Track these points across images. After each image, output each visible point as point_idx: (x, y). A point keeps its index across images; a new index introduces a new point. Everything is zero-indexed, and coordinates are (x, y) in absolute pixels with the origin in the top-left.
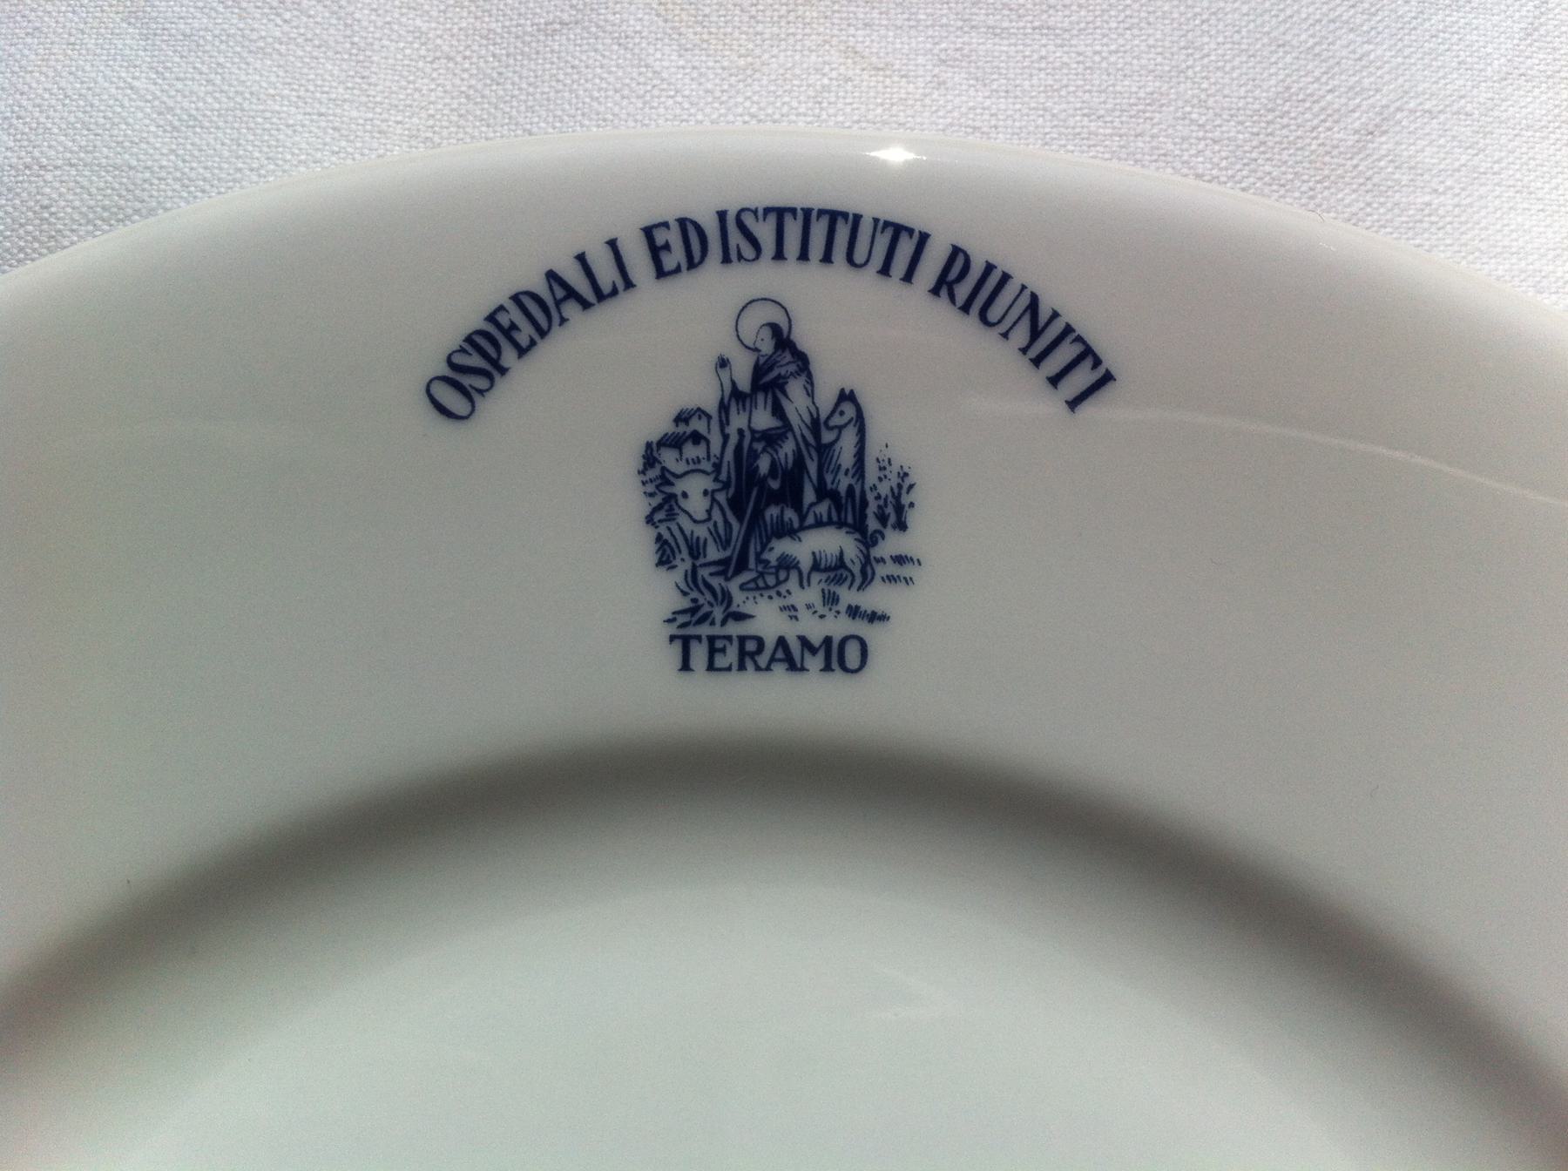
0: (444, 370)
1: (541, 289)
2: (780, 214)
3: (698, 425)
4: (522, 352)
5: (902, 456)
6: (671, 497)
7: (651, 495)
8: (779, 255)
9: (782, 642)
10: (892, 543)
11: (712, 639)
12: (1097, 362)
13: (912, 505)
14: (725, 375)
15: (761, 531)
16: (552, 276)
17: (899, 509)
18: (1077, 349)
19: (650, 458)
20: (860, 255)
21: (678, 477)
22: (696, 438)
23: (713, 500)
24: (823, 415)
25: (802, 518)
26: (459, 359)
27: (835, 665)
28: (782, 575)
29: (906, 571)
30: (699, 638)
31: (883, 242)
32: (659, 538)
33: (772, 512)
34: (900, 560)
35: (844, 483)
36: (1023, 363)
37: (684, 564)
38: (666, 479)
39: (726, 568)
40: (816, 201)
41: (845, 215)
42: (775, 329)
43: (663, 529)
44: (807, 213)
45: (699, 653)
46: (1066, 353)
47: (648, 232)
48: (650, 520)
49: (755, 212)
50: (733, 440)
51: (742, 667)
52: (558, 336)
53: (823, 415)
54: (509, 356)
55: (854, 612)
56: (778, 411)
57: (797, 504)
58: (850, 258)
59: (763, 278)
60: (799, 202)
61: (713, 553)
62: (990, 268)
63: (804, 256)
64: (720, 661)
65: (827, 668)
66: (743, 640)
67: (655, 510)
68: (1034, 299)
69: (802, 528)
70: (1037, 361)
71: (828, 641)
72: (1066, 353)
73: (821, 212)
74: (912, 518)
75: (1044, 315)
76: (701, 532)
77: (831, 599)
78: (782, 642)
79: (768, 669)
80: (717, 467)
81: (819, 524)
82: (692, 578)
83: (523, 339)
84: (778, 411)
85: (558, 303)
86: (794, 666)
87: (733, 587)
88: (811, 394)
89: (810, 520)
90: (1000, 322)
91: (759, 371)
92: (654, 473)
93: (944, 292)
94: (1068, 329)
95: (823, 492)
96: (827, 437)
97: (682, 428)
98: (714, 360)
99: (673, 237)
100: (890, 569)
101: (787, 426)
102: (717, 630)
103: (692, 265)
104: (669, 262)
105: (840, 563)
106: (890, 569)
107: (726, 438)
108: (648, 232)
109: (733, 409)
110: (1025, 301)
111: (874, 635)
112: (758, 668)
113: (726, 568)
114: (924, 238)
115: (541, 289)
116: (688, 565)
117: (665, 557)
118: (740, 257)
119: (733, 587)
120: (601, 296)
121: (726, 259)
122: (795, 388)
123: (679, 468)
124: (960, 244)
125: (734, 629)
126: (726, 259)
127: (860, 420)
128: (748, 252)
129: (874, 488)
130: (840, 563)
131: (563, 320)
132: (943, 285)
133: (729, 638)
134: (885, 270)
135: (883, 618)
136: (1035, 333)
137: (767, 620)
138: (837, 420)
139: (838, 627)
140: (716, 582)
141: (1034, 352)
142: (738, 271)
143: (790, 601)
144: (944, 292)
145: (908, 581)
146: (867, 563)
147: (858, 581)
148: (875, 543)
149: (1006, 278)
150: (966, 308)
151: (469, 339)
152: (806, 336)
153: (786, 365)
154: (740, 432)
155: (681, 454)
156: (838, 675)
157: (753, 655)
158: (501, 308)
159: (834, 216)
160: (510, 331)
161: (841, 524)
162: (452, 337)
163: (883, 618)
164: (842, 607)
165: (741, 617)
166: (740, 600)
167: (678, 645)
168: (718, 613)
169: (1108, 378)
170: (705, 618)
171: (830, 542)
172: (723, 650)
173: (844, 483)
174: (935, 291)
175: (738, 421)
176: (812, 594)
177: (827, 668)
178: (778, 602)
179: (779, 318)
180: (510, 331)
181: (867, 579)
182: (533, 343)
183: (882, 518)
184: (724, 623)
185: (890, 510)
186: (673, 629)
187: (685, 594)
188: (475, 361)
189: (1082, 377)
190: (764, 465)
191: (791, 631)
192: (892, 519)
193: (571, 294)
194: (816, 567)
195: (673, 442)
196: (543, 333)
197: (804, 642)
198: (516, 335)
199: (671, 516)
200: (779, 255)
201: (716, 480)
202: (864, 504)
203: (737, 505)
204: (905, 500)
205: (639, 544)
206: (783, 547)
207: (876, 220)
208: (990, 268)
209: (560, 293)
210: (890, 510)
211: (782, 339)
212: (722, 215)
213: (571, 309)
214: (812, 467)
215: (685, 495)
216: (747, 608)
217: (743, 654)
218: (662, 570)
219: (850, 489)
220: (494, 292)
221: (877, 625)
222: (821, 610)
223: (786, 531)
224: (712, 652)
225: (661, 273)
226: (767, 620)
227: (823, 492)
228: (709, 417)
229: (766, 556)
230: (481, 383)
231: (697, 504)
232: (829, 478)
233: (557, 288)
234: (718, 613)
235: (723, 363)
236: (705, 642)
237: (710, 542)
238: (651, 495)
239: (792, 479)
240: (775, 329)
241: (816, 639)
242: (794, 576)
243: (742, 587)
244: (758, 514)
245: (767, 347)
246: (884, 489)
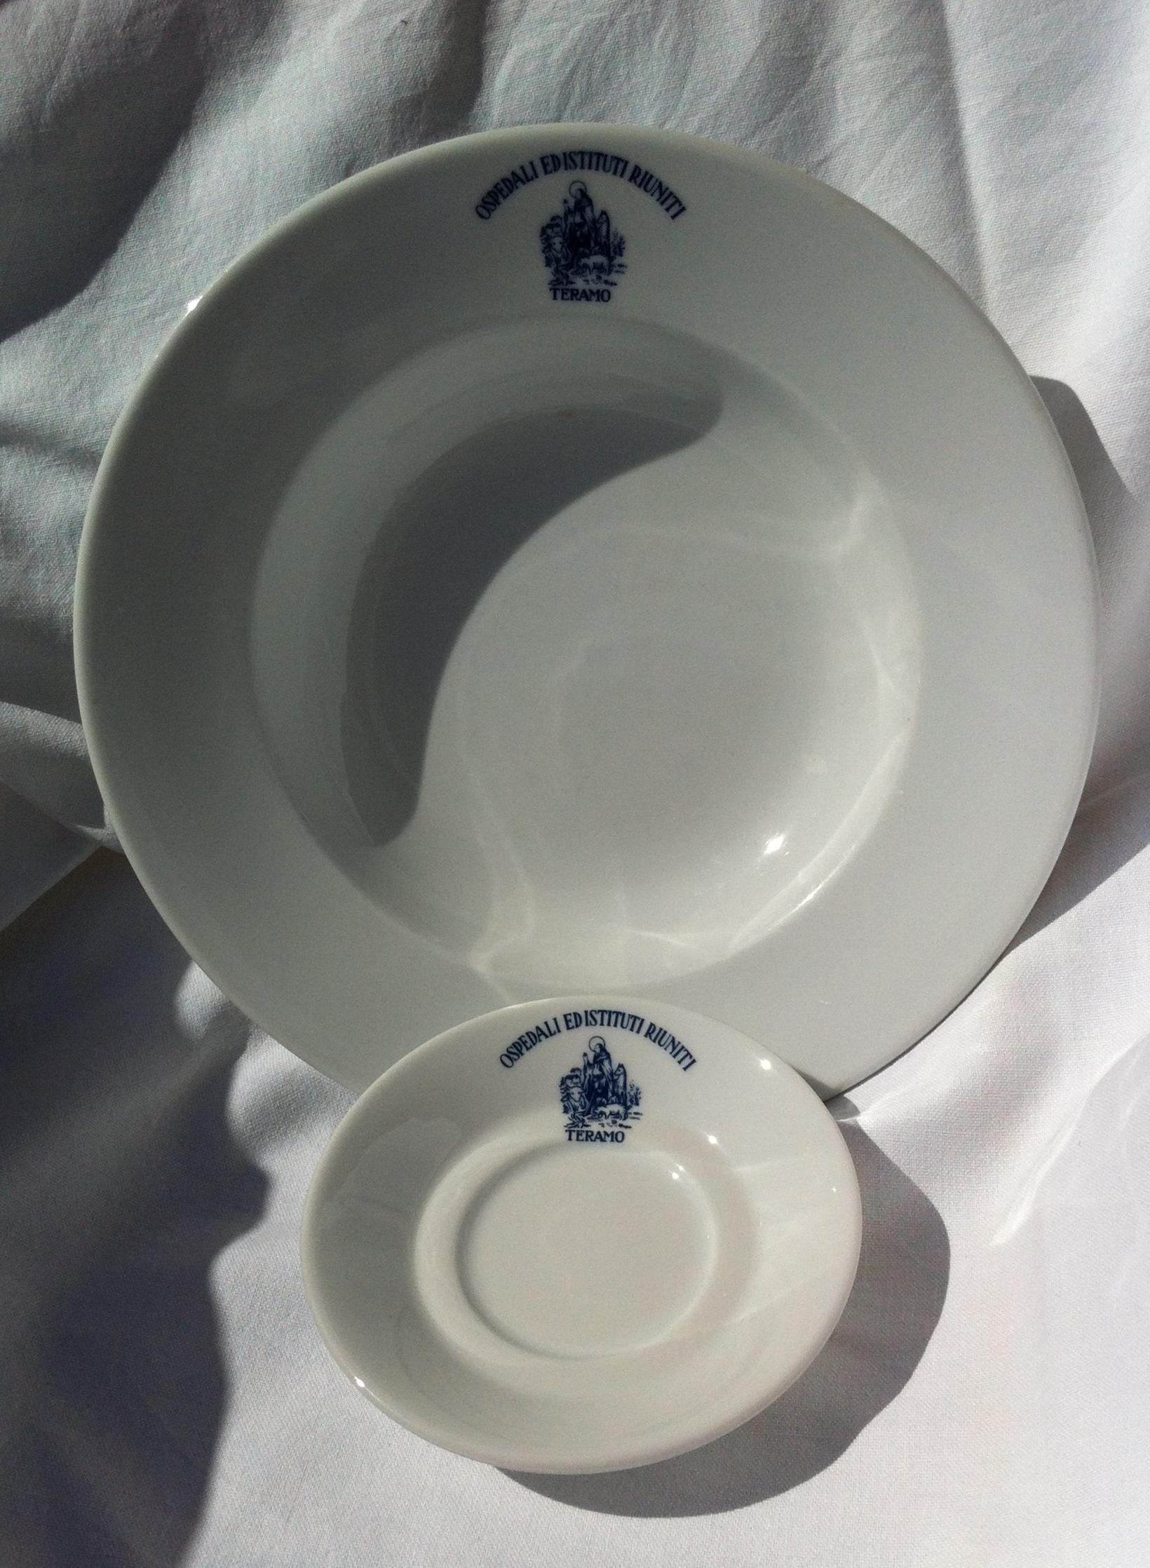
0: (506, 1053)
1: (510, 177)
2: (582, 153)
3: (558, 221)
4: (528, 1049)
5: (638, 1083)
6: (568, 1094)
7: (563, 1093)
8: (602, 1024)
9: (599, 1133)
10: (618, 260)
11: (578, 1131)
12: (691, 1057)
13: (624, 248)
14: (585, 1058)
15: (595, 1105)
16: (538, 1028)
17: (637, 1099)
18: (674, 200)
19: (563, 1081)
20: (625, 1025)
21: (572, 1088)
22: (577, 1077)
23: (581, 1096)
24: (597, 218)
25: (608, 1101)
26: (486, 200)
27: (614, 1139)
28: (584, 270)
29: (621, 269)
30: (574, 1131)
31: (631, 1021)
32: (564, 1106)
33: (599, 1099)
34: (621, 266)
35: (620, 1091)
36: (670, 1057)
37: (554, 265)
38: (567, 1088)
39: (583, 1114)
40: (594, 148)
41: (621, 1013)
42: (581, 190)
43: (566, 1103)
44: (610, 1012)
45: (559, 294)
46: (683, 1054)
47: (565, 1016)
48: (562, 1100)
49: (595, 1011)
50: (588, 1077)
51: (587, 1140)
52: (516, 192)
53: (597, 218)
54: (501, 199)
55: (621, 1125)
56: (601, 1069)
57: (589, 247)
58: (622, 1026)
59: (598, 1030)
60: (608, 1009)
61: (563, 262)
62: (661, 1029)
63: (609, 1024)
64: (580, 1138)
65: (612, 1140)
66: (587, 1132)
67: (564, 1097)
68: (673, 1038)
69: (608, 1104)
70: (674, 1056)
71: (612, 1133)
72: (683, 1054)
73: (614, 1012)
74: (641, 1102)
75: (676, 1043)
76: (559, 256)
77: (599, 278)
78: (599, 1133)
79: (595, 1141)
80: (583, 1086)
81: (613, 1103)
82: (573, 1116)
83: (505, 194)
84: (601, 1069)
85: (539, 1036)
86: (602, 1140)
87: (585, 1118)
88: (592, 211)
89: (610, 1102)
90: (664, 1045)
91: (596, 1057)
92: (544, 237)
93: (648, 1036)
94: (683, 1047)
95: (614, 1094)
96: (615, 1077)
97: (573, 1074)
98: (582, 1054)
99: (550, 160)
100: (617, 268)
101: (603, 1074)
102: (580, 1129)
103: (577, 1026)
104: (571, 1025)
105: (618, 1113)
106: (633, 1115)
107: (585, 1076)
108: (565, 1016)
109: (569, 216)
110: (671, 1039)
111: (611, 289)
112: (592, 1140)
113: (583, 1114)
114: (643, 1020)
115: (510, 177)
116: (572, 1113)
117: (548, 264)
118: (591, 1024)
119: (569, 273)
120: (551, 1035)
121: (587, 1025)
122: (606, 1063)
123: (553, 235)
124: (653, 1022)
125: (585, 1129)
126: (587, 1025)
127: (625, 1073)
128: (593, 1023)
129: (629, 1093)
130: (618, 1113)
131: (540, 1041)
132: (648, 1034)
133: (583, 1131)
134: (632, 1030)
135: (615, 284)
136: (674, 1048)
137: (580, 284)
138: (618, 1073)
139: (616, 1129)
140: (564, 271)
141: (674, 1053)
142: (590, 1028)
143: (587, 278)
144: (648, 1036)
145: (623, 273)
146: (611, 266)
147: (623, 1118)
148: (613, 260)
149: (665, 1032)
150: (654, 1041)
151: (513, 1044)
152: (609, 1049)
153: (585, 203)
154: (590, 1075)
155: (553, 230)
156: (616, 1143)
157: (590, 1136)
158: (523, 1036)
159: (618, 1013)
160: (525, 1043)
161: (619, 1103)
162: (509, 1043)
163: (615, 284)
164: (618, 1124)
165: (572, 283)
166: (587, 1122)
167: (552, 291)
168: (581, 1125)
169: (694, 1061)
170: (562, 282)
171: (599, 259)
172: (581, 1135)
173: (620, 1091)
174: (646, 1036)
175: (570, 219)
176: (593, 276)
177: (612, 1140)
178: (583, 278)
179: (600, 1041)
180: (525, 1043)
181: (610, 272)
182: (531, 1047)
183: (632, 1102)
184: (582, 1127)
185: (634, 1100)
186: (550, 286)
187: (570, 1119)
188: (514, 1050)
189: (676, 209)
190: (596, 1085)
191: (587, 287)
192: (618, 253)
193: (543, 1033)
194: (611, 1114)
195: (550, 226)
196: (534, 1044)
197: (591, 292)
198: (503, 192)
199: (550, 251)
200: (602, 1024)
201: (564, 239)
202: (626, 1098)
203: (588, 1097)
204: (638, 1096)
205: (540, 259)
206: (584, 261)
207: (629, 1015)
208: (661, 1029)
209: (540, 1033)
210: (634, 1100)
211: (603, 1048)
212: (564, 154)
213: (542, 1037)
214: (593, 235)
215: (573, 1094)
216: (590, 1124)
217: (587, 1135)
218: (547, 268)
219: (622, 1093)
220: (522, 1031)
221: (628, 1129)
222: (611, 1124)
223: (588, 256)
224: (563, 294)
225: (568, 1028)
226: (580, 284)
227: (597, 243)
228: (561, 218)
229: (579, 264)
230: (516, 1057)
231: (558, 246)
232: (616, 1090)
233: (515, 178)
234: (565, 281)
235: (585, 1055)
236: (576, 1133)
237: (562, 259)
238: (563, 1093)
239: (605, 1089)
240: (600, 1045)
241: (609, 1133)
242: (588, 271)
243: (588, 1118)
244: (595, 1099)
245: (598, 1050)
246: (632, 1093)
